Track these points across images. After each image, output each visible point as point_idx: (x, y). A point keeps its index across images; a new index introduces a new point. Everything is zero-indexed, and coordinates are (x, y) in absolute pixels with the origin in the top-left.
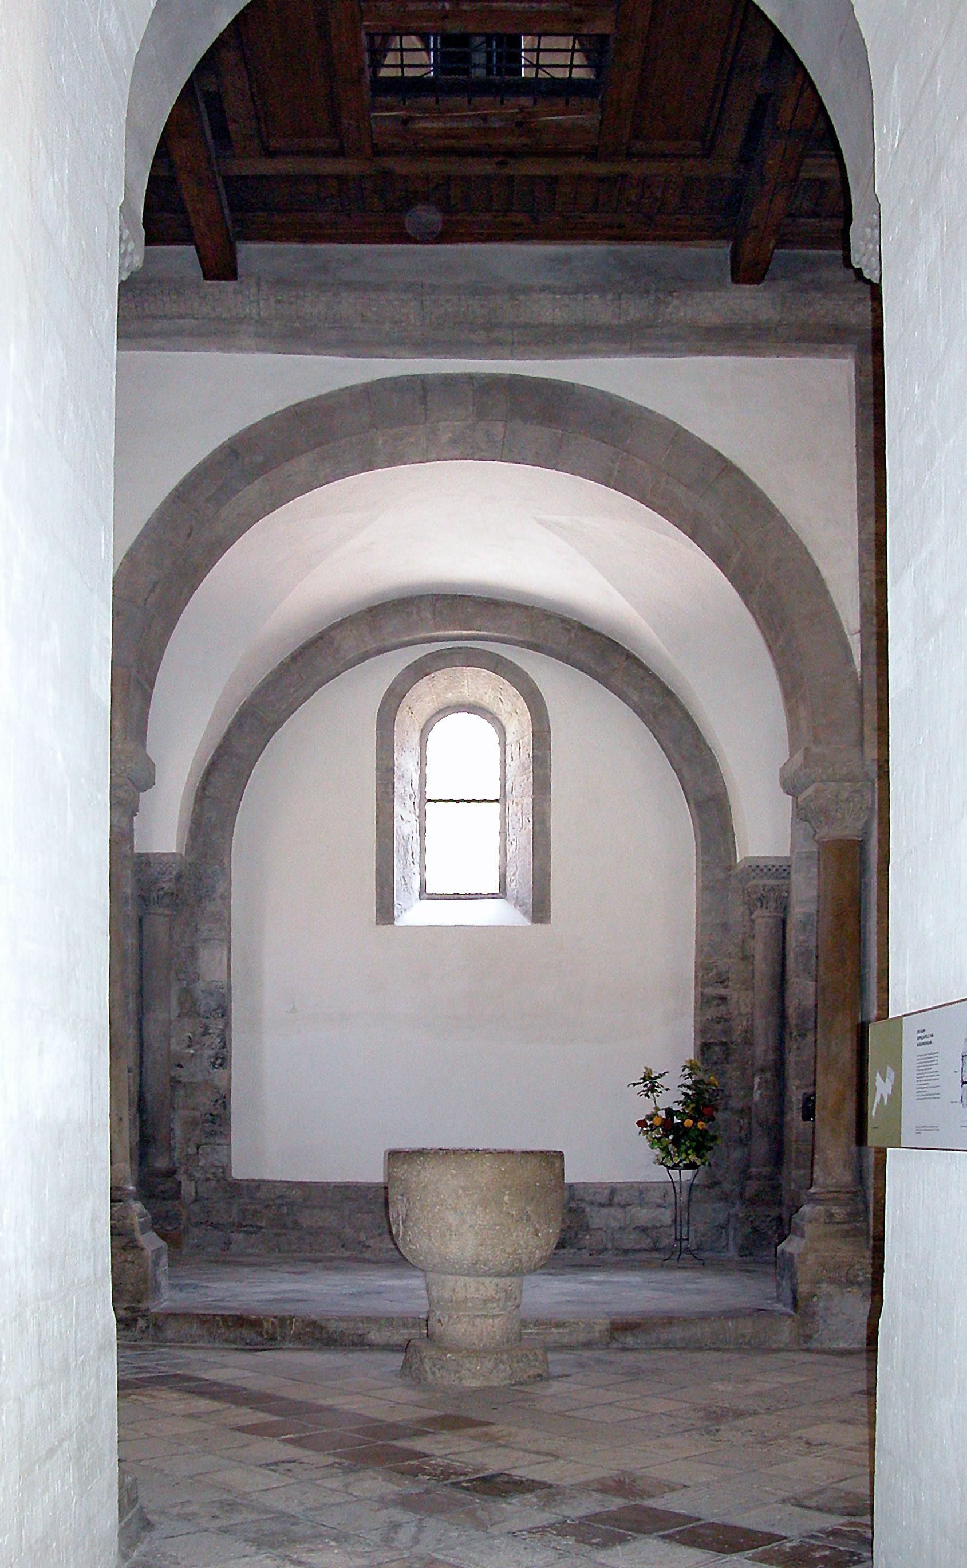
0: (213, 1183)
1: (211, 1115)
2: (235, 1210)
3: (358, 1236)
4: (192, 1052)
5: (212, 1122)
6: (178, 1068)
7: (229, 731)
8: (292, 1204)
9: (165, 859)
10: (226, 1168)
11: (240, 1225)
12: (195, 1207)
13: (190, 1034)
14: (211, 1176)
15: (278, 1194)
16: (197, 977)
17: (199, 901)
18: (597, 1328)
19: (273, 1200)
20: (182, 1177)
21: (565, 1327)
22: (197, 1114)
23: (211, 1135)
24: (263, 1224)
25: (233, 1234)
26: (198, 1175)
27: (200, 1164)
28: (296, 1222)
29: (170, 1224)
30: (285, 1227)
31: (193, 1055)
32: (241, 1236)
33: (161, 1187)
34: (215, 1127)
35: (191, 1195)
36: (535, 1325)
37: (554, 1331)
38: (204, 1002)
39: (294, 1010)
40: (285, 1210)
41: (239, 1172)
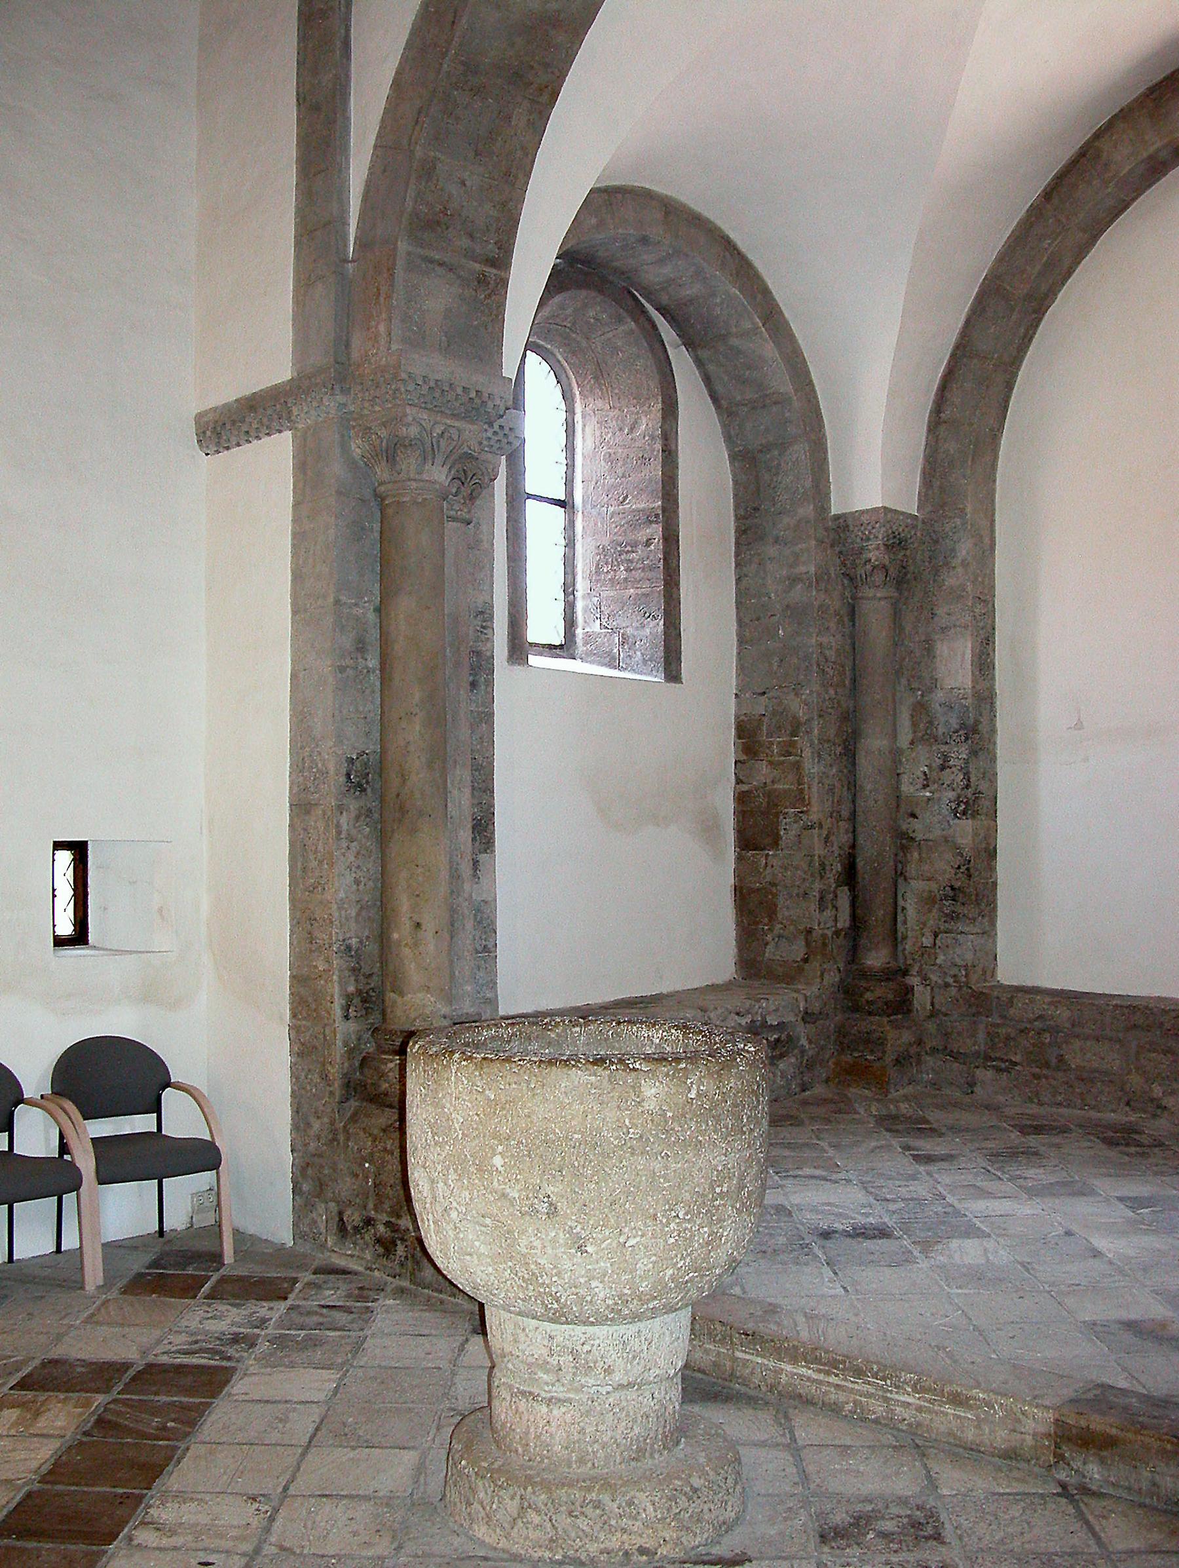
0: (953, 991)
1: (952, 888)
2: (981, 1036)
3: (1151, 1090)
4: (928, 794)
5: (954, 900)
6: (911, 819)
7: (968, 322)
8: (1054, 1030)
9: (864, 519)
10: (990, 970)
11: (988, 1058)
12: (931, 1027)
13: (926, 769)
14: (951, 980)
15: (1038, 1013)
16: (934, 684)
17: (936, 572)
18: (1029, 1425)
19: (1030, 1021)
20: (914, 980)
21: (970, 1408)
22: (934, 886)
23: (952, 918)
24: (1017, 1058)
25: (978, 1072)
26: (934, 978)
27: (938, 961)
28: (1061, 1059)
29: (872, 1052)
30: (1047, 1065)
31: (929, 799)
32: (990, 1074)
33: (868, 996)
34: (959, 909)
35: (925, 1008)
36: (915, 1390)
37: (948, 1409)
38: (943, 719)
39: (1079, 726)
40: (1046, 1037)
41: (1009, 972)
